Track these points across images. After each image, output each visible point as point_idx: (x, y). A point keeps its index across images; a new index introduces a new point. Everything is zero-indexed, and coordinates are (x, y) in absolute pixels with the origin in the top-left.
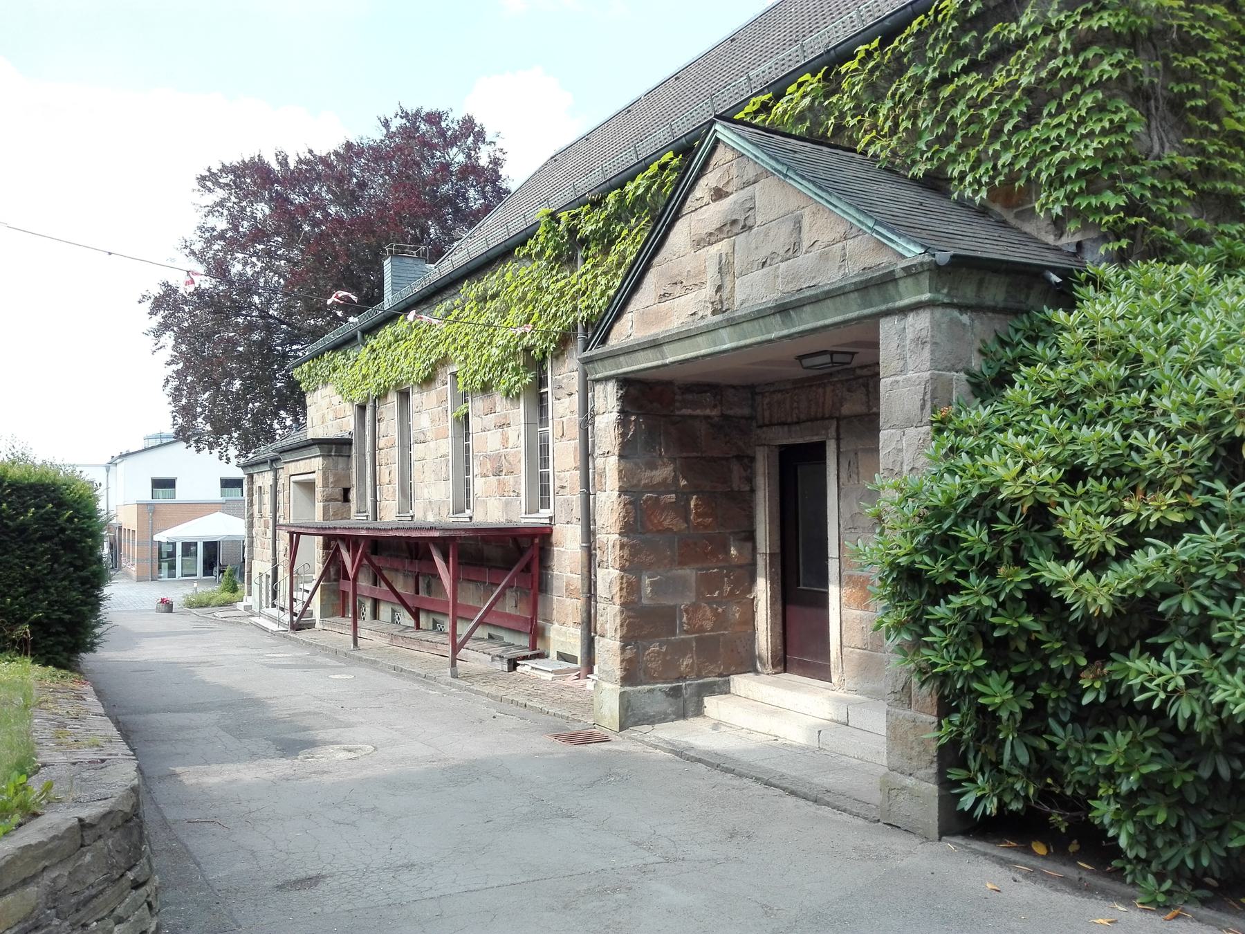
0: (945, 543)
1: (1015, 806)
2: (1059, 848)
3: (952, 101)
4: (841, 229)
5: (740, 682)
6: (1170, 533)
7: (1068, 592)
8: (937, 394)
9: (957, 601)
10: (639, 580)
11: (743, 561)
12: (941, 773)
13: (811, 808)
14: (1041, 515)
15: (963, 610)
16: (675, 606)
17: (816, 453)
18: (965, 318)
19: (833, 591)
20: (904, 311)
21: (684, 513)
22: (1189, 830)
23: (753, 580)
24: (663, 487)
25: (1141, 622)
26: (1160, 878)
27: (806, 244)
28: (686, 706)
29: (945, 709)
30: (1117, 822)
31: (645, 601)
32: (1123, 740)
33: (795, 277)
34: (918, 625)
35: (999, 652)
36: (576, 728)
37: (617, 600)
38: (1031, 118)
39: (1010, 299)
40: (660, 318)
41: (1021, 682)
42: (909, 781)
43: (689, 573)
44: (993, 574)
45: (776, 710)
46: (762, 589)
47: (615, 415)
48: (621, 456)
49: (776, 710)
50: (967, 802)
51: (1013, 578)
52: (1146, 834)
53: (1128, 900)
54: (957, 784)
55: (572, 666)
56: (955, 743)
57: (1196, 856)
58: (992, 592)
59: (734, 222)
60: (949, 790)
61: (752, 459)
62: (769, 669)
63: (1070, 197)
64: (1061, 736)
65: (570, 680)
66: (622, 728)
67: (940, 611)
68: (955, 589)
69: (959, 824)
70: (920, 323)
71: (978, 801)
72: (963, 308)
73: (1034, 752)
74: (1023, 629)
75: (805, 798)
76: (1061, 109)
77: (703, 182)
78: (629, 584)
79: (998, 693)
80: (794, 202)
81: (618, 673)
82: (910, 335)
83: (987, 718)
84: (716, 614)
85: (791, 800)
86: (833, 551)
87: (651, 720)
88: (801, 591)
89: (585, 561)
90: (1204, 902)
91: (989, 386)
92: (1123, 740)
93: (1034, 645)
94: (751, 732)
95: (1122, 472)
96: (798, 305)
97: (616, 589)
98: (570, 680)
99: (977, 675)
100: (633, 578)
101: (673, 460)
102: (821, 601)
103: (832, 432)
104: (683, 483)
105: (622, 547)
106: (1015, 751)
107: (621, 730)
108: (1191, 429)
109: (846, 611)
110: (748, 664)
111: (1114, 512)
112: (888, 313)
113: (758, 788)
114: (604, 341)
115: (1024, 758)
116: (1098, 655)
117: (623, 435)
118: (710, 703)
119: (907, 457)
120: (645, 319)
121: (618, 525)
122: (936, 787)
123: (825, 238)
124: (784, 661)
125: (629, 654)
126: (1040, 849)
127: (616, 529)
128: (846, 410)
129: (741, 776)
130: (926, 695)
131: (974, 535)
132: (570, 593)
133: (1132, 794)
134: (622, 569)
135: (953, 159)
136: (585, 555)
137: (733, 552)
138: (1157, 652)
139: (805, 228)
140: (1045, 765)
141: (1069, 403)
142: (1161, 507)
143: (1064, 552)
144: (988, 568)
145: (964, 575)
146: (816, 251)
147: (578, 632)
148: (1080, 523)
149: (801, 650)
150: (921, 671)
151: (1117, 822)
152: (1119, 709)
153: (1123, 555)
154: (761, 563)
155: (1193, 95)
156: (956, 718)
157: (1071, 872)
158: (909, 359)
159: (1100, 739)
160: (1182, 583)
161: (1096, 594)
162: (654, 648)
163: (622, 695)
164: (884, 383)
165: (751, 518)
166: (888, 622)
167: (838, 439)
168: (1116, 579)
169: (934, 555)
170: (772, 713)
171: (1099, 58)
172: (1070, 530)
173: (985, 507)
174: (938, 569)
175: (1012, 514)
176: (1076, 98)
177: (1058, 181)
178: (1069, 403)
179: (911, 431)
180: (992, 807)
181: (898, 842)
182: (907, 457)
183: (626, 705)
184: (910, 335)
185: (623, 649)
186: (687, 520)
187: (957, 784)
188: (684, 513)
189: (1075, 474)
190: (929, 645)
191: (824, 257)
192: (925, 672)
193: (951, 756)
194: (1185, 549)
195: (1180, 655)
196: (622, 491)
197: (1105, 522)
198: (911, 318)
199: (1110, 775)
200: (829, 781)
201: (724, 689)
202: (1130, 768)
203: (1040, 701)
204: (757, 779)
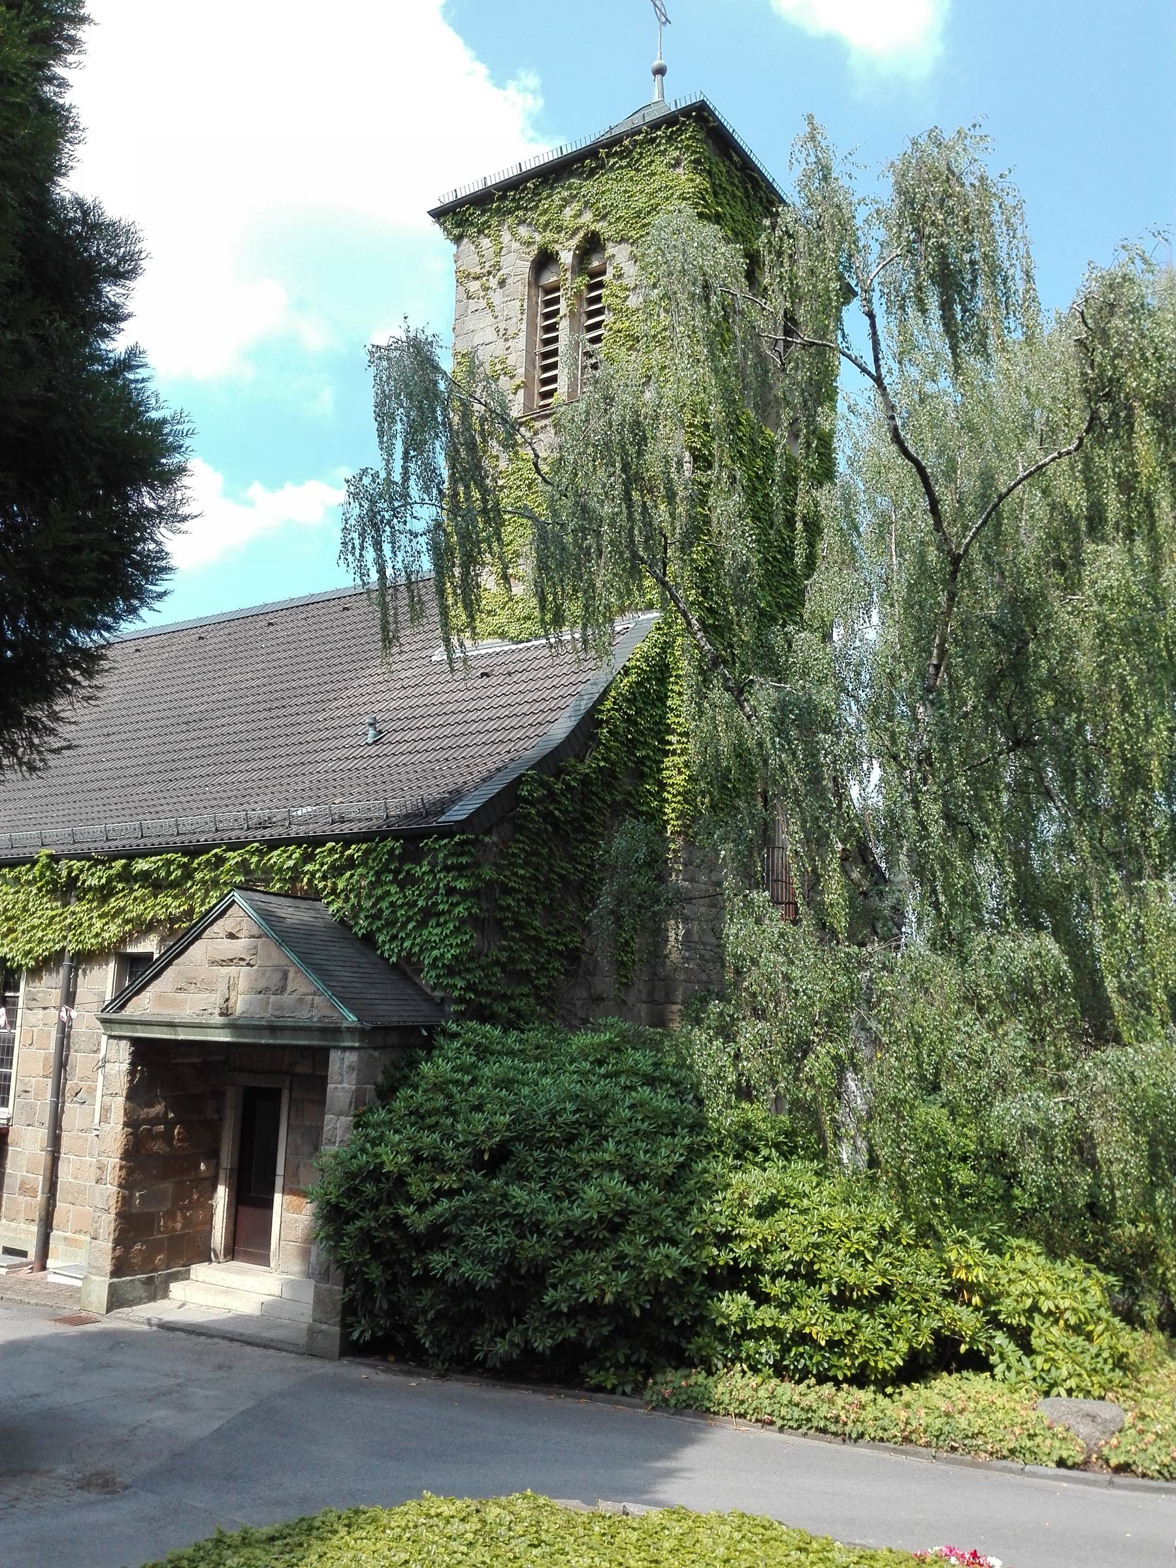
0: (353, 1192)
1: (380, 1334)
2: (401, 1358)
3: (380, 899)
4: (312, 989)
5: (199, 1271)
6: (451, 1194)
7: (408, 1221)
8: (358, 1098)
9: (358, 1224)
10: (132, 1195)
11: (208, 1175)
12: (343, 1319)
13: (264, 1351)
14: (400, 1180)
15: (361, 1228)
16: (153, 1214)
17: (274, 1096)
18: (376, 1054)
19: (278, 1197)
20: (345, 1049)
21: (167, 1136)
22: (457, 1337)
23: (215, 1189)
24: (154, 1121)
25: (437, 1237)
26: (443, 1363)
27: (289, 989)
28: (156, 1291)
29: (347, 1282)
30: (425, 1335)
31: (134, 1211)
32: (430, 1293)
33: (281, 1008)
34: (337, 1237)
35: (377, 1251)
36: (67, 1313)
37: (113, 1211)
38: (422, 924)
39: (399, 1048)
40: (174, 1004)
41: (387, 1266)
42: (324, 1327)
43: (168, 1186)
44: (377, 1209)
45: (229, 1291)
46: (222, 1194)
47: (125, 1066)
48: (129, 1098)
49: (229, 1291)
50: (355, 1335)
51: (386, 1212)
52: (437, 1342)
53: (428, 1376)
54: (351, 1325)
55: (24, 1260)
56: (352, 1300)
57: (458, 1348)
58: (376, 1219)
59: (242, 959)
60: (346, 1327)
61: (223, 1094)
62: (221, 1258)
63: (438, 976)
64: (403, 1293)
65: (24, 1272)
66: (108, 1311)
67: (350, 1228)
68: (356, 1216)
69: (351, 1349)
70: (351, 1058)
71: (362, 1332)
72: (375, 1049)
73: (390, 1302)
74: (389, 1238)
75: (258, 1345)
76: (438, 925)
77: (220, 922)
78: (124, 1197)
79: (375, 1273)
80: (284, 962)
81: (109, 1268)
82: (346, 1063)
83: (368, 1286)
84: (185, 1218)
85: (249, 1349)
86: (280, 1170)
87: (130, 1304)
88: (252, 1200)
89: (49, 1163)
90: (462, 1372)
91: (386, 1094)
92: (430, 1293)
93: (393, 1245)
94: (209, 1307)
95: (439, 1162)
96: (283, 1029)
97: (113, 1202)
98: (24, 1272)
99: (365, 1263)
100: (127, 1193)
101: (165, 1099)
102: (269, 1205)
103: (287, 1084)
104: (171, 1115)
105: (121, 1168)
106: (382, 1303)
107: (108, 1311)
108: (464, 1145)
109: (285, 1214)
110: (204, 1255)
111: (433, 1180)
112: (337, 1048)
113: (224, 1343)
114: (122, 1007)
115: (385, 1307)
116: (421, 1251)
117: (131, 1082)
118: (174, 1286)
119: (339, 1133)
120: (160, 998)
121: (120, 1151)
122: (338, 1328)
123: (303, 990)
124: (232, 1252)
125: (118, 1253)
126: (391, 1358)
127: (119, 1153)
128: (299, 1069)
129: (211, 1336)
130: (338, 1274)
131: (370, 1189)
132: (24, 1190)
133: (433, 1320)
134: (120, 1186)
135: (379, 930)
136: (49, 1158)
137: (203, 1167)
138: (443, 1250)
139: (290, 979)
140: (395, 1309)
141: (418, 1115)
142: (449, 1181)
143: (409, 1200)
144: (375, 1206)
145: (363, 1210)
146: (295, 996)
147: (34, 1228)
148: (418, 1187)
149: (249, 1241)
150: (337, 1262)
151: (425, 1335)
152: (427, 1279)
153: (434, 1202)
154: (222, 1175)
155: (507, 919)
156: (353, 1287)
157: (405, 1368)
158: (344, 1075)
159: (421, 1294)
160: (455, 1218)
161: (419, 1222)
162: (138, 1247)
163: (111, 1285)
164: (330, 1086)
165: (218, 1140)
166: (322, 1234)
167: (291, 1090)
168: (428, 1216)
169: (350, 1199)
170: (227, 1293)
171: (458, 904)
172: (413, 1189)
173: (376, 1174)
174: (350, 1206)
175: (388, 1179)
176: (446, 922)
177: (433, 966)
178: (418, 1115)
179: (343, 1118)
180: (367, 1336)
181: (316, 1363)
182: (339, 1133)
183: (113, 1290)
184: (346, 1063)
185: (114, 1249)
186: (170, 1145)
187: (351, 1325)
188: (167, 1136)
189: (418, 1159)
190: (344, 1248)
191: (300, 1001)
192: (340, 1262)
193: (348, 1310)
194: (456, 1202)
195: (452, 1252)
196: (126, 1124)
197: (428, 1186)
198: (347, 1054)
199: (424, 1312)
200: (272, 1334)
201: (185, 1276)
202: (432, 1307)
203: (394, 1275)
204: (224, 1338)
